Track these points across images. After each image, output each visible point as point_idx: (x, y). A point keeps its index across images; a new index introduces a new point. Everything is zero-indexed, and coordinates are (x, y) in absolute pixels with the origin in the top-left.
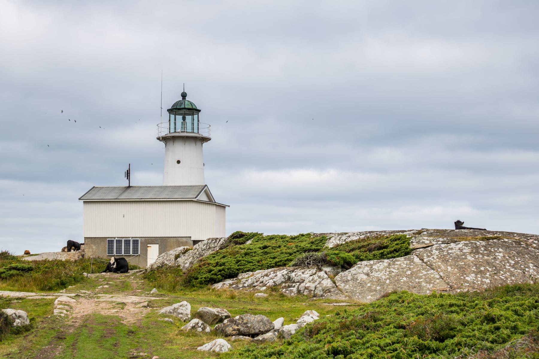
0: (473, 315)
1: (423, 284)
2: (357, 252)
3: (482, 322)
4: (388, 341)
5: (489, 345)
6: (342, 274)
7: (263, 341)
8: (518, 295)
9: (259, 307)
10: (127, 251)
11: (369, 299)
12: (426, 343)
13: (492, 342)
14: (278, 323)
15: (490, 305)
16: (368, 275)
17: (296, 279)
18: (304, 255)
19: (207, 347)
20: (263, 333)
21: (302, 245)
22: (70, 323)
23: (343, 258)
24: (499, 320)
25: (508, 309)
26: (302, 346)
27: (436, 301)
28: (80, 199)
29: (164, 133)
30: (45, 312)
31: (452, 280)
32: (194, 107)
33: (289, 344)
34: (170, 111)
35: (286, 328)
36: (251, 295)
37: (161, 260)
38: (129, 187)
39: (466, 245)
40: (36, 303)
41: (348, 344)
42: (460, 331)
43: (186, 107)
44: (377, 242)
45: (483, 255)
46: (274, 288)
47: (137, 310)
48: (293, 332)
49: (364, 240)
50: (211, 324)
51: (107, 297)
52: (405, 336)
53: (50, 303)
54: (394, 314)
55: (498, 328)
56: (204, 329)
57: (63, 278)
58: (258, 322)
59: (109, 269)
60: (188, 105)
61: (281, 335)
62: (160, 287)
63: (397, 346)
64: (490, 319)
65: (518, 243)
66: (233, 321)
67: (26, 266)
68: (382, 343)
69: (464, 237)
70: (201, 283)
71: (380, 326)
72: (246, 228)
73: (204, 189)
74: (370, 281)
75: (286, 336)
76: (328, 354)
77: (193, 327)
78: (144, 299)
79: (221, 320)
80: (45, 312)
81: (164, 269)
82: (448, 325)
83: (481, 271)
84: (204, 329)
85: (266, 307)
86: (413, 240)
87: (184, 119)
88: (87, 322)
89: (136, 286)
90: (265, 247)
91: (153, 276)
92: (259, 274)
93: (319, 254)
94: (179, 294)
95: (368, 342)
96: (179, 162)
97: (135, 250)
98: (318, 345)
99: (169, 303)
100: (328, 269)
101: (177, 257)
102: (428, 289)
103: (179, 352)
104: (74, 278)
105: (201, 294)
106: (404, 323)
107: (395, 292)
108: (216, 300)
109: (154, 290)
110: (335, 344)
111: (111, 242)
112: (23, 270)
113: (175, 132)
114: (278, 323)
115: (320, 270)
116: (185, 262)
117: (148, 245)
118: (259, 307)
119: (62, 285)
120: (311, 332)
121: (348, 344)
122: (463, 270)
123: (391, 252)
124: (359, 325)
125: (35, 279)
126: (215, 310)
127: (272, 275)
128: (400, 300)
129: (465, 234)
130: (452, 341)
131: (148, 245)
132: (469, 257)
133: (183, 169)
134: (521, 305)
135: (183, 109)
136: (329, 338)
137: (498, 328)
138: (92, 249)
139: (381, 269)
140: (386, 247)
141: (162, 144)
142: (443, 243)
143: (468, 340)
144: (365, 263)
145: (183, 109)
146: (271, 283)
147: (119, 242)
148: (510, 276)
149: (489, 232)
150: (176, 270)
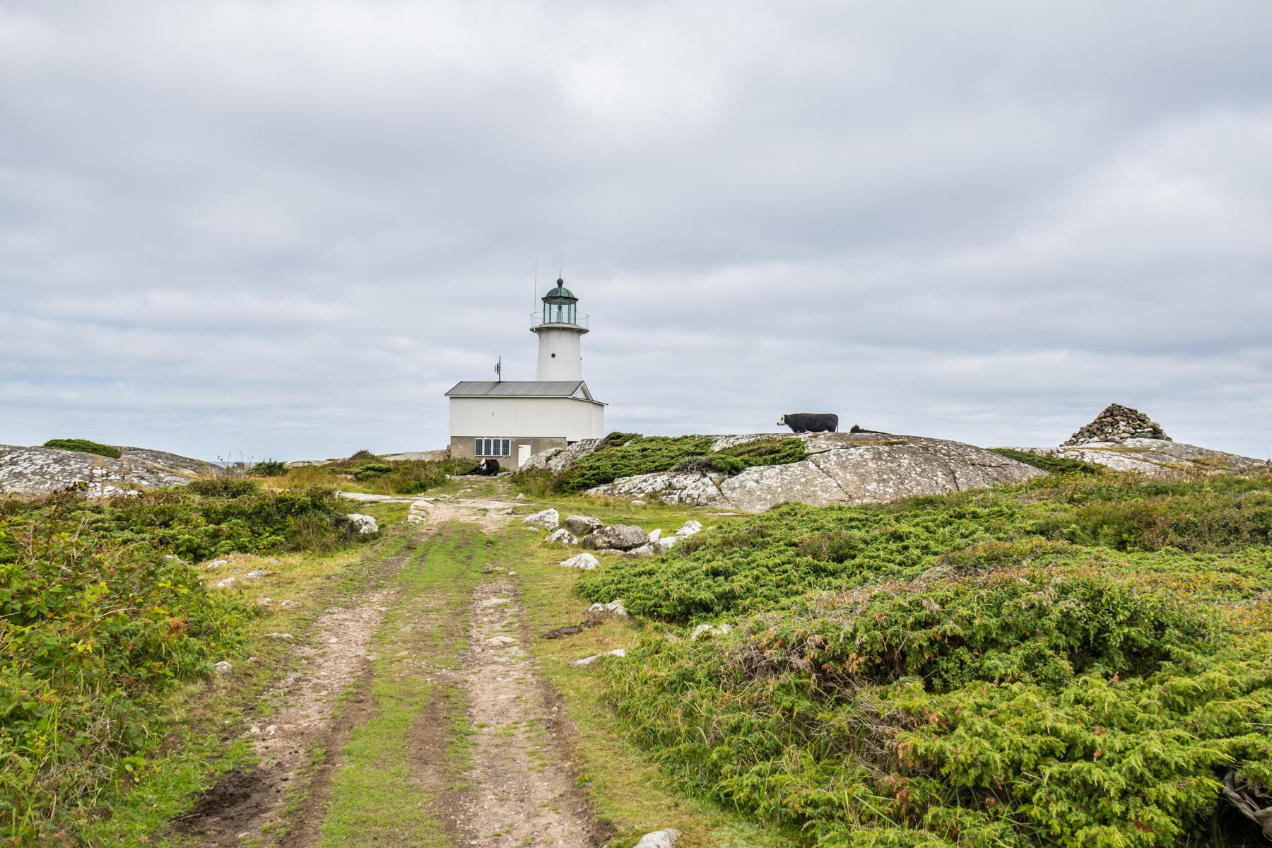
0: (877, 532)
1: (819, 493)
2: (746, 457)
3: (888, 541)
4: (777, 561)
5: (897, 567)
6: (729, 480)
7: (636, 556)
8: (929, 509)
9: (636, 516)
10: (497, 451)
11: (759, 509)
12: (821, 564)
13: (900, 565)
14: (654, 535)
15: (897, 520)
16: (757, 482)
17: (678, 485)
18: (687, 459)
19: (570, 563)
20: (636, 546)
21: (685, 448)
22: (424, 531)
24: (908, 538)
25: (917, 524)
26: (677, 565)
27: (835, 515)
29: (538, 323)
30: (399, 518)
31: (851, 489)
33: (663, 561)
34: (546, 300)
35: (663, 541)
36: (628, 503)
37: (530, 463)
39: (867, 450)
40: (391, 508)
41: (730, 564)
42: (862, 550)
44: (769, 445)
45: (886, 461)
46: (653, 495)
47: (500, 517)
48: (670, 546)
49: (753, 443)
50: (578, 535)
51: (468, 502)
52: (798, 555)
54: (784, 529)
55: (906, 548)
56: (570, 541)
58: (632, 534)
59: (476, 471)
61: (657, 549)
62: (527, 492)
63: (788, 567)
64: (898, 537)
65: (926, 449)
66: (603, 532)
67: (384, 466)
68: (771, 563)
69: (865, 441)
70: (573, 488)
71: (768, 543)
72: (624, 430)
74: (758, 489)
75: (663, 550)
76: (707, 575)
77: (559, 539)
78: (508, 505)
79: (592, 530)
80: (399, 518)
81: (534, 472)
82: (847, 542)
83: (884, 480)
84: (570, 541)
85: (644, 516)
86: (809, 444)
87: (560, 308)
88: (443, 531)
89: (502, 490)
90: (644, 450)
91: (521, 480)
92: (637, 479)
93: (703, 458)
94: (548, 500)
95: (753, 561)
97: (506, 452)
98: (695, 564)
99: (536, 511)
100: (713, 475)
101: (548, 459)
102: (824, 499)
103: (539, 567)
105: (572, 501)
106: (796, 540)
107: (787, 503)
108: (586, 509)
109: (521, 496)
110: (714, 564)
111: (479, 442)
112: (380, 470)
114: (654, 535)
115: (705, 476)
116: (557, 465)
118: (636, 516)
119: (422, 488)
120: (688, 548)
121: (730, 564)
122: (863, 479)
124: (744, 542)
125: (393, 481)
126: (585, 519)
127: (651, 480)
128: (792, 513)
129: (867, 438)
130: (852, 562)
132: (870, 464)
133: (565, 362)
134: (933, 521)
136: (709, 556)
137: (906, 548)
139: (772, 475)
140: (778, 452)
141: (536, 335)
142: (842, 447)
143: (872, 562)
144: (754, 468)
145: (560, 297)
146: (650, 489)
147: (488, 442)
148: (917, 486)
149: (893, 436)
150: (546, 473)
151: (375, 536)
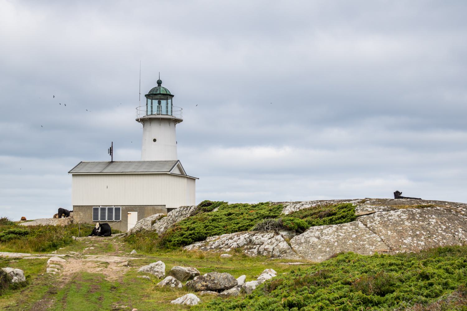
23: (297, 223)
28: (69, 172)
29: (143, 115)
32: (168, 93)
34: (148, 96)
38: (112, 162)
43: (161, 92)
51: (93, 257)
53: (44, 263)
57: (55, 241)
60: (163, 91)
73: (177, 164)
87: (159, 103)
96: (155, 140)
97: (117, 217)
104: (64, 241)
111: (96, 210)
113: (152, 114)
117: (129, 212)
119: (54, 247)
123: (339, 219)
131: (129, 212)
133: (159, 147)
135: (158, 94)
138: (80, 215)
140: (334, 214)
141: (141, 125)
145: (159, 94)
147: (103, 209)
151: (23, 285)
